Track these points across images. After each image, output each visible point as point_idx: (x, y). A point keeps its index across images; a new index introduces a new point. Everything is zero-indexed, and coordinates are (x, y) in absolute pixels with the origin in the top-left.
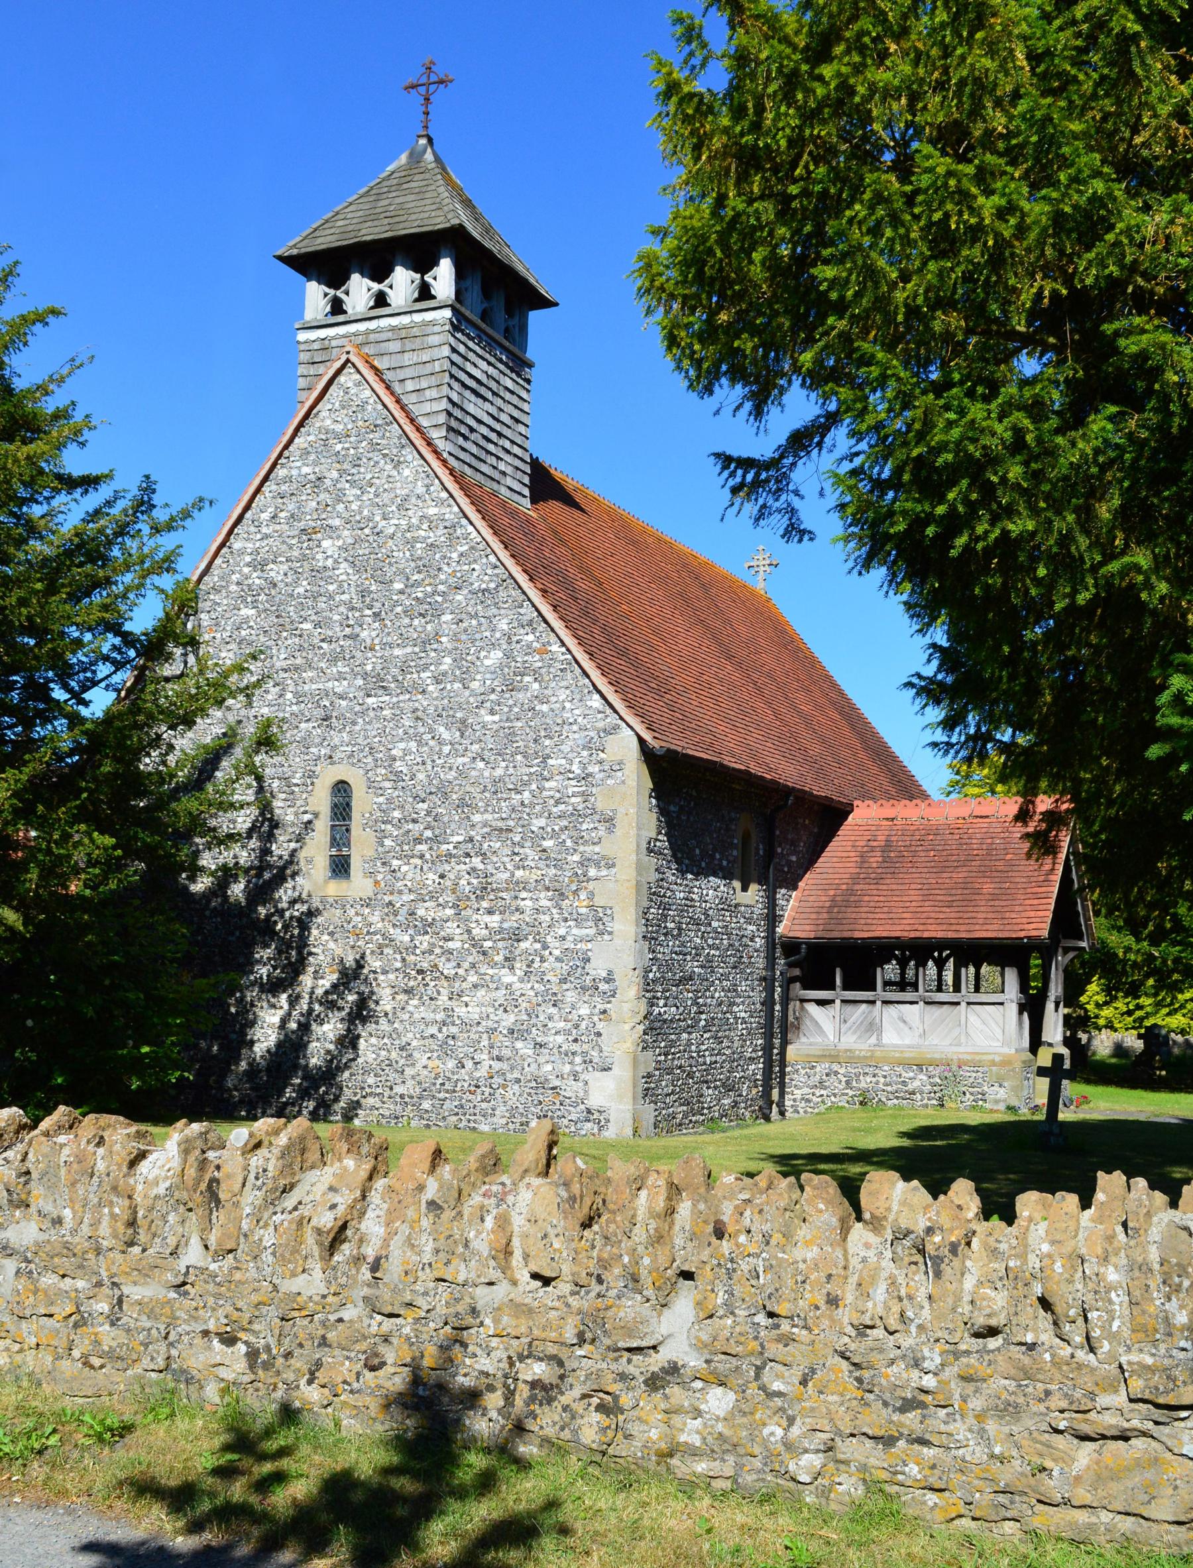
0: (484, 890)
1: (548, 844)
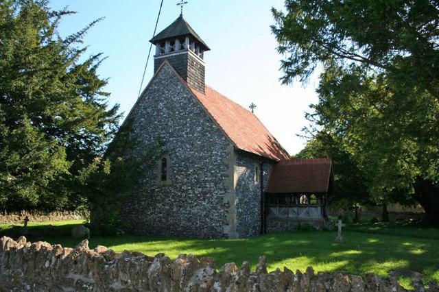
0: (198, 182)
1: (213, 171)
